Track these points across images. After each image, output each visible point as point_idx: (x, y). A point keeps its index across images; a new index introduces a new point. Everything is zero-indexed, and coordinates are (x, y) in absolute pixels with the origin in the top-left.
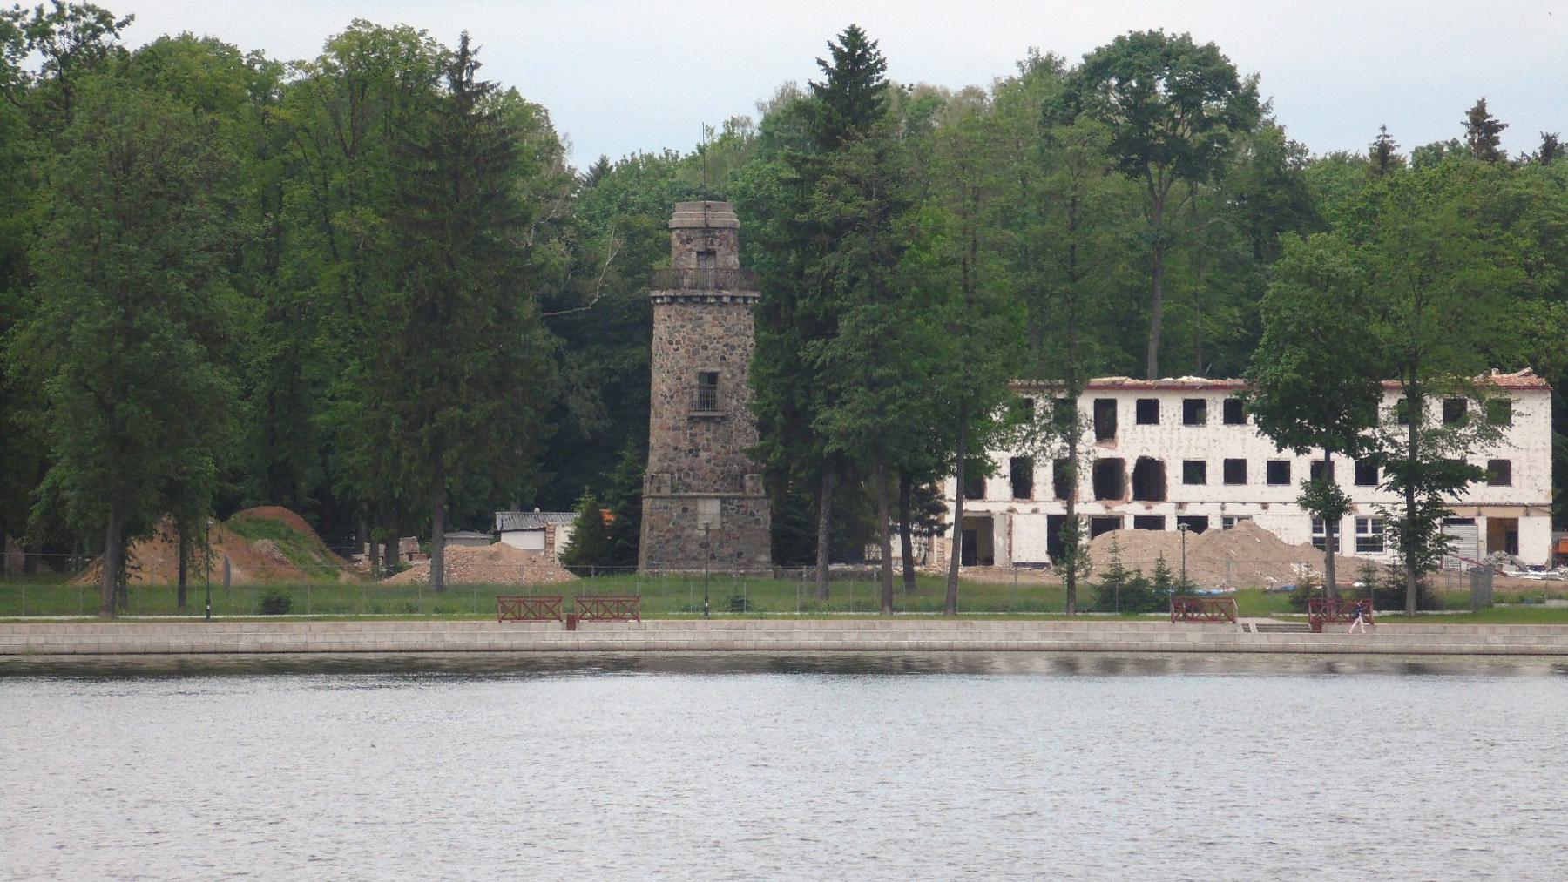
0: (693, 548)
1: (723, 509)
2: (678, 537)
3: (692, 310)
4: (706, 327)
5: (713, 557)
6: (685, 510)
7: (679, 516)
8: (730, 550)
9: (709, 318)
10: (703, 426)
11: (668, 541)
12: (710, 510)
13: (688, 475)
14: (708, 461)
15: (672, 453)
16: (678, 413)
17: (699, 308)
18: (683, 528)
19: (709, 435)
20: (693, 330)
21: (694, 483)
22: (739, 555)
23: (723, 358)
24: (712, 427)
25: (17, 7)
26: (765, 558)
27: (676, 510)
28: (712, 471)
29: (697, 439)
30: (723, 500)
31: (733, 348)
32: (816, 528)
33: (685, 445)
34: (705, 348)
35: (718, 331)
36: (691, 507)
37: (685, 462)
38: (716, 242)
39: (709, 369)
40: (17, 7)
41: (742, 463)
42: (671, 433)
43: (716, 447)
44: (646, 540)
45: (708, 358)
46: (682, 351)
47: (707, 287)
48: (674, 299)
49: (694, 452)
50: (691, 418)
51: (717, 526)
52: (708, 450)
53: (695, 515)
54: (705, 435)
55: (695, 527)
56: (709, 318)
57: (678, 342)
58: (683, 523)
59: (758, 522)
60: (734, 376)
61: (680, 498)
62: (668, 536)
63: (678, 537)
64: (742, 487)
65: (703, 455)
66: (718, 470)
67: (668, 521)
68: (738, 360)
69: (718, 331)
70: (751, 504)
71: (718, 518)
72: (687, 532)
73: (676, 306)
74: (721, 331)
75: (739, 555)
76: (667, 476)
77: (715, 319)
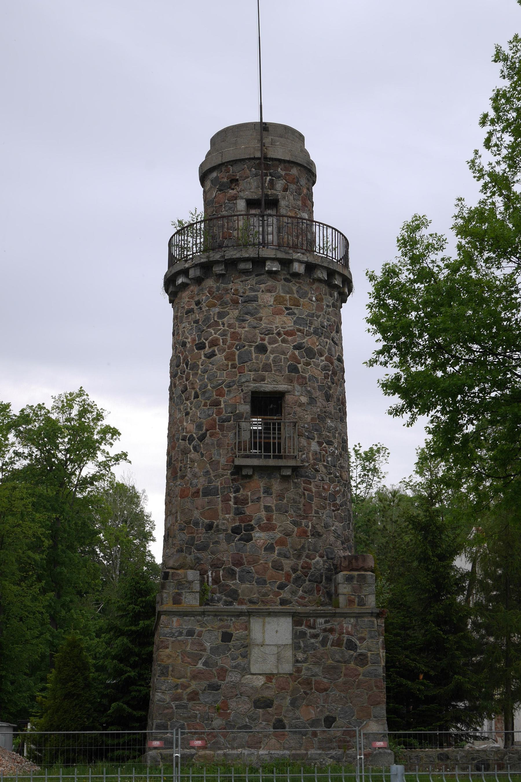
0: (240, 707)
1: (298, 636)
2: (215, 687)
3: (238, 285)
4: (263, 313)
5: (279, 725)
6: (227, 637)
7: (215, 650)
8: (313, 713)
9: (269, 298)
10: (259, 483)
11: (194, 696)
12: (273, 636)
13: (231, 574)
14: (270, 548)
15: (201, 535)
16: (214, 464)
17: (252, 281)
18: (223, 672)
19: (271, 501)
20: (241, 320)
21: (243, 588)
22: (330, 721)
23: (293, 369)
24: (276, 486)
25: (43, 404)
26: (377, 727)
27: (210, 640)
28: (277, 566)
29: (248, 510)
30: (298, 619)
31: (310, 353)
32: (181, 742)
33: (227, 520)
34: (262, 349)
35: (286, 322)
36: (237, 633)
37: (226, 550)
38: (280, 185)
39: (267, 387)
40: (43, 404)
41: (329, 556)
42: (201, 501)
43: (283, 522)
44: (161, 695)
45: (267, 368)
46: (220, 357)
47: (264, 244)
48: (384, 586)
49: (243, 532)
50: (238, 470)
51: (287, 668)
52: (268, 528)
53: (246, 647)
54: (262, 499)
55: (245, 670)
56: (269, 298)
57: (214, 343)
58: (224, 661)
59: (362, 660)
60: (312, 401)
61: (216, 614)
62: (194, 685)
63: (215, 687)
64: (332, 597)
65: (260, 537)
66: (287, 564)
67: (196, 658)
68: (319, 375)
69: (286, 322)
70: (348, 625)
71: (289, 654)
72: (233, 677)
73: (210, 283)
74: (289, 323)
75: (330, 721)
76: (192, 575)
77: (279, 300)
